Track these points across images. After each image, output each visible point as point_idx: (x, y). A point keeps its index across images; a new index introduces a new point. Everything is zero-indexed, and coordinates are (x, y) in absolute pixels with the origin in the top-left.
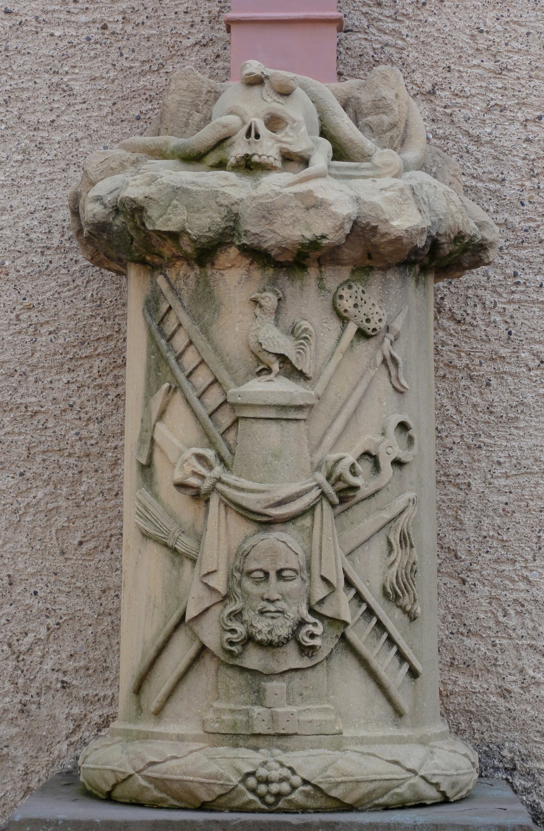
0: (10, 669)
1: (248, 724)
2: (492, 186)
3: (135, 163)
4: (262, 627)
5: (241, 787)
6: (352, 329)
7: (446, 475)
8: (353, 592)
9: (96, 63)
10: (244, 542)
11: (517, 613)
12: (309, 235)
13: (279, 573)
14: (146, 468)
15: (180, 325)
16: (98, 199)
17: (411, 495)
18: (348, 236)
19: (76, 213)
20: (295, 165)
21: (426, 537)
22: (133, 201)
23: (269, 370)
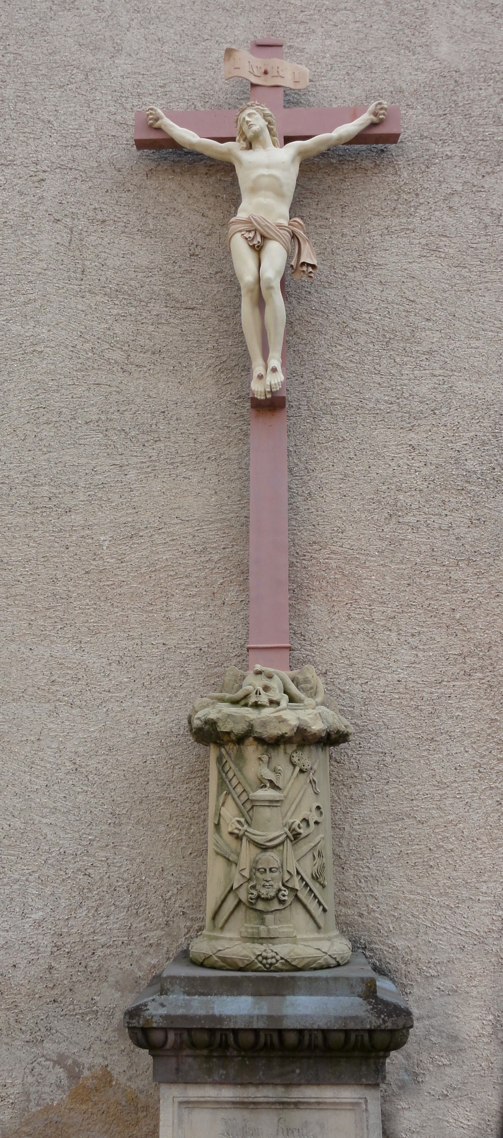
0: (162, 906)
1: (259, 933)
2: (349, 709)
3: (213, 704)
4: (264, 892)
5: (256, 961)
6: (297, 769)
7: (335, 824)
8: (300, 877)
9: (197, 663)
10: (256, 856)
11: (365, 881)
12: (280, 733)
13: (270, 869)
14: (217, 826)
15: (230, 768)
16: (199, 718)
17: (322, 836)
18: (295, 733)
19: (190, 722)
20: (274, 705)
21: (328, 853)
22: (212, 719)
23: (265, 786)
